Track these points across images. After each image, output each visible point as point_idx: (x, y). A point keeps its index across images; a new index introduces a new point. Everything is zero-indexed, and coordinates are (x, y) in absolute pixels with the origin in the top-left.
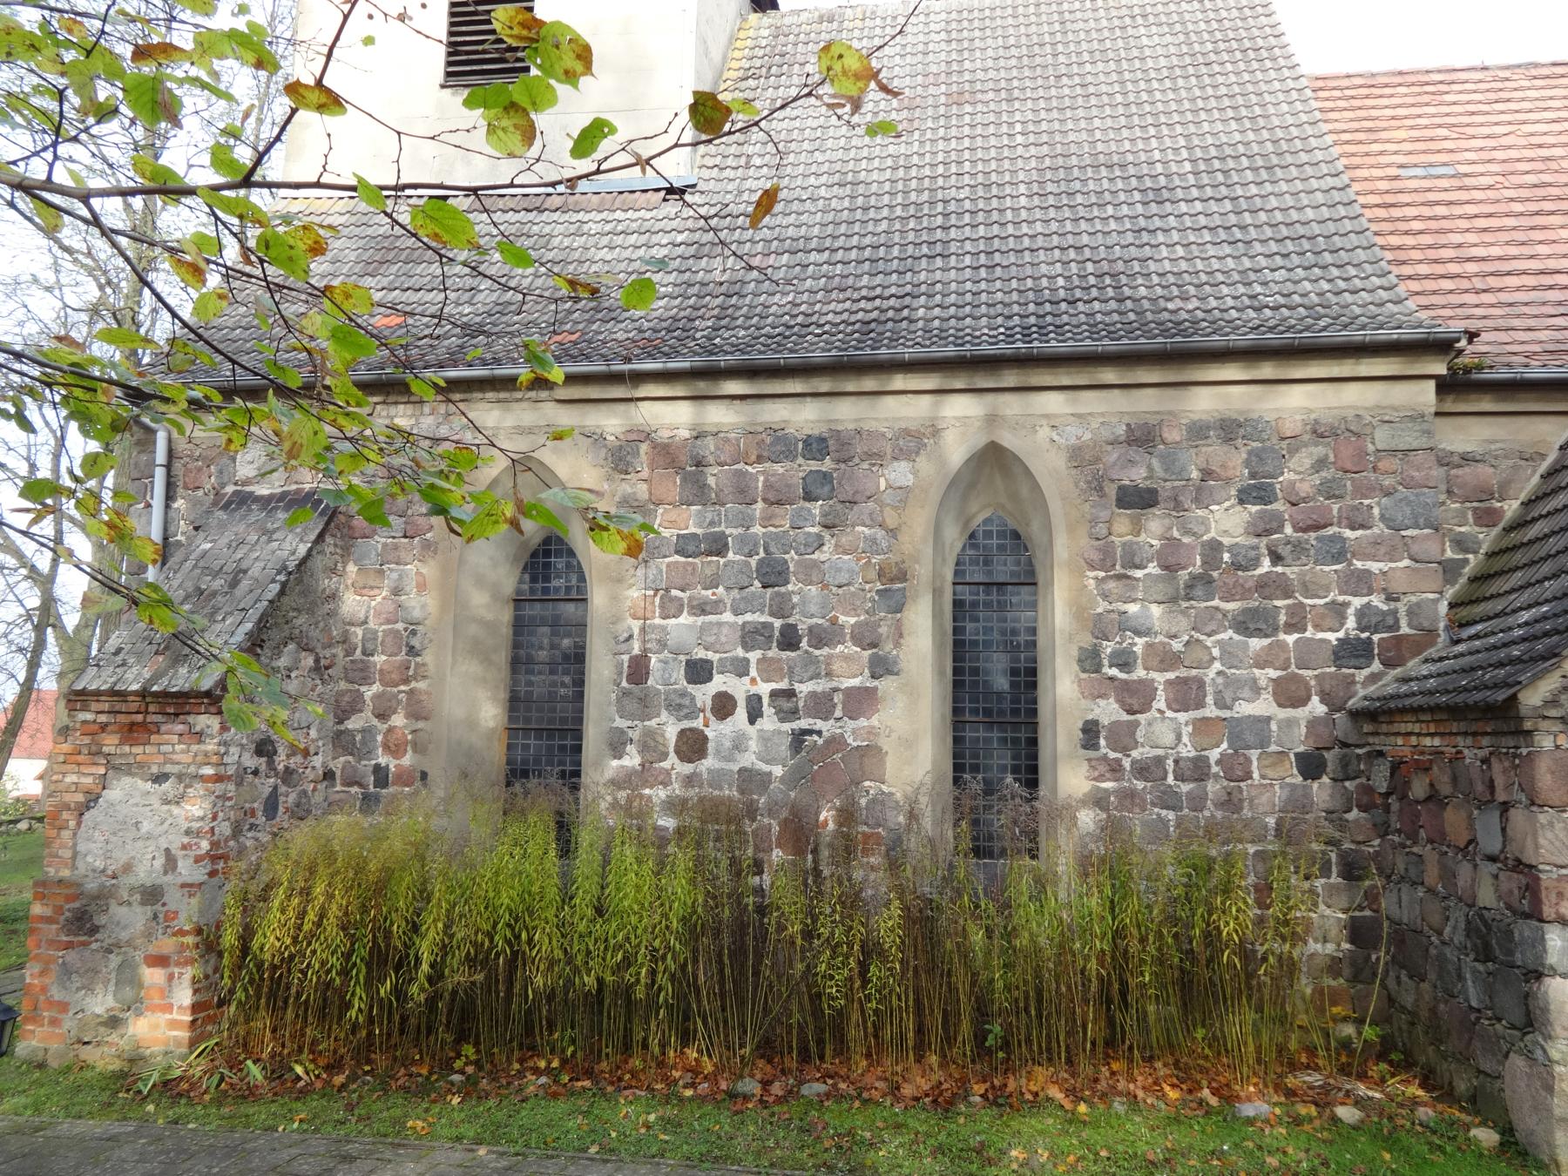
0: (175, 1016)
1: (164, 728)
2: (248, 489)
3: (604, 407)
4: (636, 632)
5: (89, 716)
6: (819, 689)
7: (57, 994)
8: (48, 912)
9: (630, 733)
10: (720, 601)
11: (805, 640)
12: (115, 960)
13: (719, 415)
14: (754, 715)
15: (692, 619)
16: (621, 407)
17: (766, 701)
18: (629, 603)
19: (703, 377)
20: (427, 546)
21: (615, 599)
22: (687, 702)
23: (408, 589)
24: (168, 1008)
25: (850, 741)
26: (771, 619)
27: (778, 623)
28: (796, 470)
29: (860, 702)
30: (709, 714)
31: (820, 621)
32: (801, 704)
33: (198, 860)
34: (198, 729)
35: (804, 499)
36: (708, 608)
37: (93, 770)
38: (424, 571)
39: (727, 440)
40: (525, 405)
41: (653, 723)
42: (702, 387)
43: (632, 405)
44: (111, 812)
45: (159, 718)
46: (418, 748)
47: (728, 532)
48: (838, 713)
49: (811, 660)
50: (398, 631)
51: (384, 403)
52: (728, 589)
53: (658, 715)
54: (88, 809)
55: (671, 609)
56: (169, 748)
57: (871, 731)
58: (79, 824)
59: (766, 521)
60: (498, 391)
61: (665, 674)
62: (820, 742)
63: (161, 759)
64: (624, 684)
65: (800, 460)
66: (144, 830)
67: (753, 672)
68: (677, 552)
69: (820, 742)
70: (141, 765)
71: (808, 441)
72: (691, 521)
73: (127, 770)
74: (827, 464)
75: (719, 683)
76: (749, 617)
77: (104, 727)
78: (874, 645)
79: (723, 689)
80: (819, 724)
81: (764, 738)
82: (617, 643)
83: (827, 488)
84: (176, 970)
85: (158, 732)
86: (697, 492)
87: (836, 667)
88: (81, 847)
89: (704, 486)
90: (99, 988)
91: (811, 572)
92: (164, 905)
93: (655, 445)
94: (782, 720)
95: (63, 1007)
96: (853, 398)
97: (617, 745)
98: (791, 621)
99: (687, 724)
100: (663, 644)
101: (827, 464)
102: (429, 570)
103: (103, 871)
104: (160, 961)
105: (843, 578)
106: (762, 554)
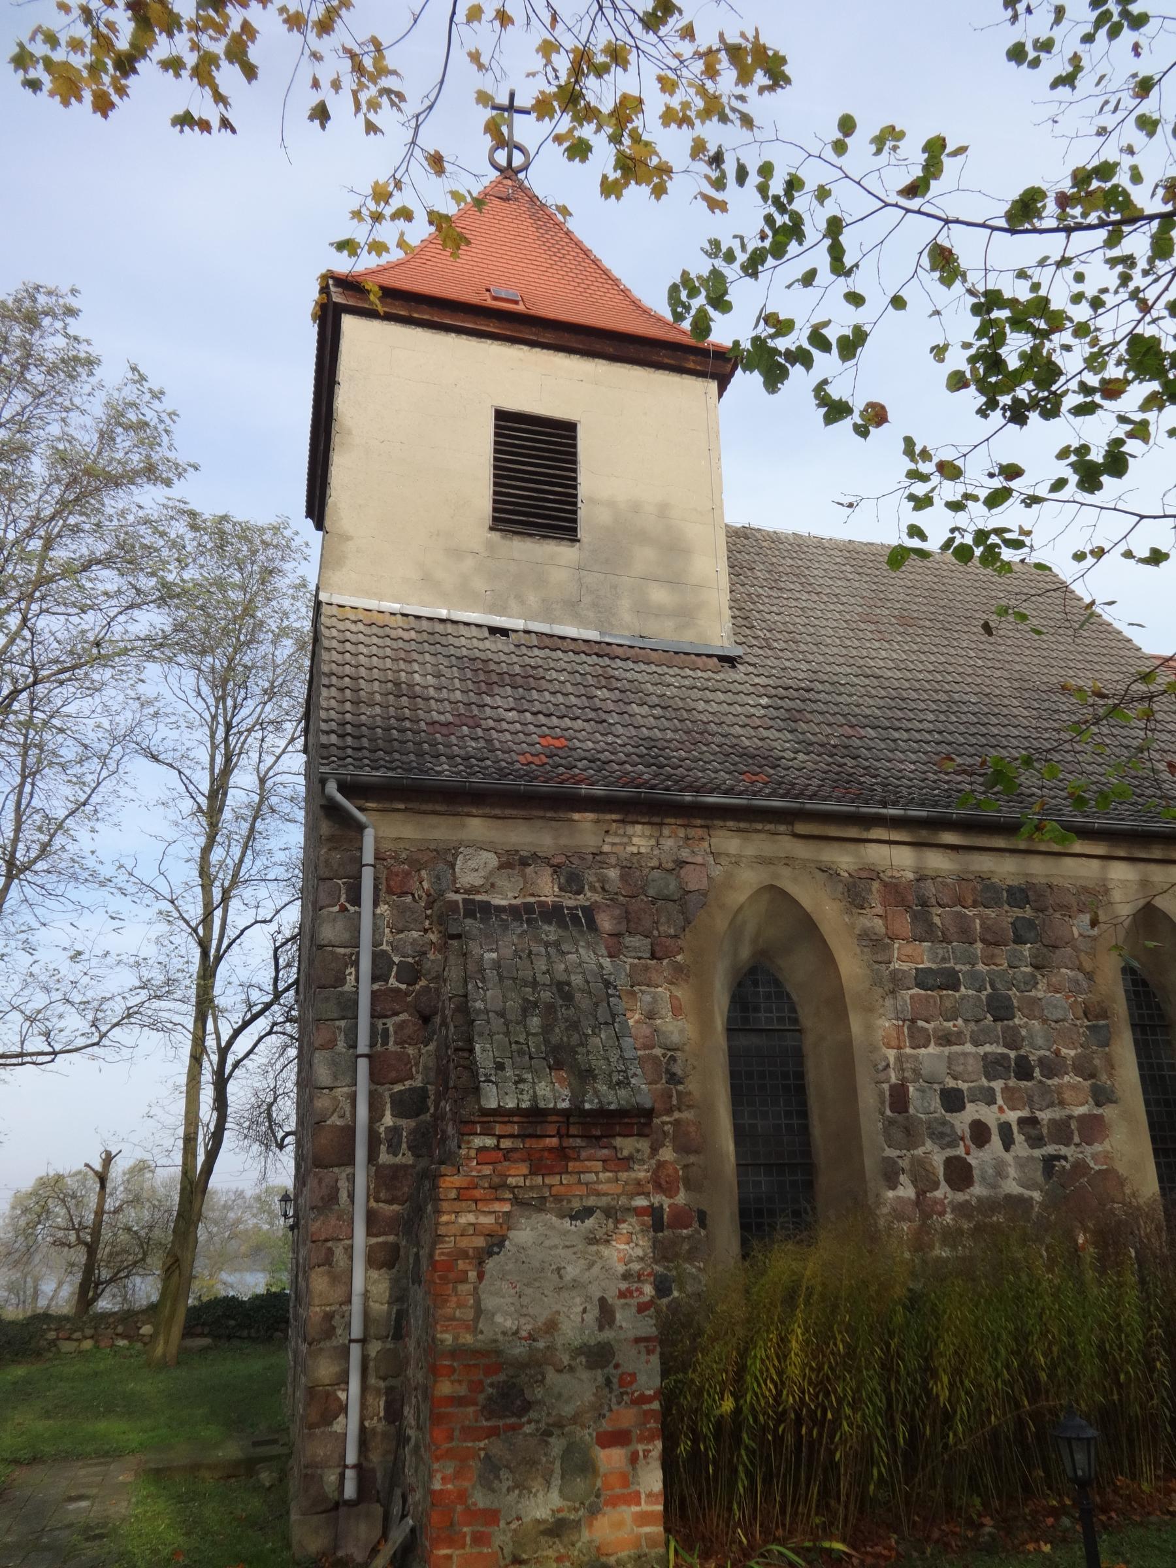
0: (645, 1507)
1: (584, 1154)
2: (478, 897)
3: (836, 845)
4: (892, 1060)
5: (490, 1142)
6: (1057, 1117)
7: (480, 1499)
8: (462, 1390)
9: (900, 1162)
10: (960, 1033)
11: (1037, 1070)
12: (557, 1445)
13: (937, 861)
14: (1008, 1143)
15: (939, 1049)
16: (851, 847)
17: (1015, 1128)
18: (881, 1033)
19: (922, 829)
20: (678, 969)
21: (869, 1028)
22: (948, 1131)
23: (663, 1012)
24: (635, 1498)
25: (1092, 1165)
26: (1006, 1051)
27: (1012, 1054)
28: (1004, 916)
29: (1092, 1128)
30: (969, 1142)
31: (1047, 1053)
32: (1045, 1131)
33: (642, 1308)
34: (626, 1153)
35: (1015, 942)
36: (953, 1039)
37: (497, 1206)
38: (679, 994)
39: (945, 885)
40: (763, 836)
41: (920, 1151)
42: (924, 835)
43: (861, 845)
44: (523, 1257)
45: (579, 1142)
46: (690, 1185)
47: (958, 967)
48: (1077, 1139)
49: (1045, 1090)
50: (656, 1057)
51: (623, 821)
52: (966, 1021)
53: (923, 1144)
54: (491, 1254)
55: (919, 1039)
56: (593, 1177)
57: (1107, 1156)
58: (481, 1276)
59: (989, 960)
60: (739, 820)
61: (924, 1104)
62: (1068, 1166)
63: (582, 1190)
64: (888, 1112)
65: (1006, 907)
66: (568, 1278)
67: (1000, 1102)
68: (918, 985)
69: (1068, 1166)
70: (558, 1199)
71: (1010, 890)
72: (924, 956)
73: (539, 1205)
74: (1028, 912)
75: (973, 1111)
76: (988, 1048)
77: (507, 1154)
78: (1092, 1076)
79: (977, 1117)
80: (1064, 1150)
81: (1021, 1163)
82: (877, 1071)
83: (1033, 934)
84: (640, 1448)
85: (578, 1159)
86: (925, 931)
87: (1068, 1095)
88: (489, 1302)
89: (932, 925)
90: (537, 1485)
91: (1033, 1007)
92: (617, 1366)
93: (886, 885)
94: (1032, 1147)
95: (492, 1516)
96: (1041, 857)
97: (891, 1178)
98: (1022, 1052)
99: (950, 1152)
100: (917, 1072)
101: (1028, 912)
102: (682, 993)
103: (516, 1333)
104: (618, 1438)
105: (1059, 1014)
106: (989, 990)
